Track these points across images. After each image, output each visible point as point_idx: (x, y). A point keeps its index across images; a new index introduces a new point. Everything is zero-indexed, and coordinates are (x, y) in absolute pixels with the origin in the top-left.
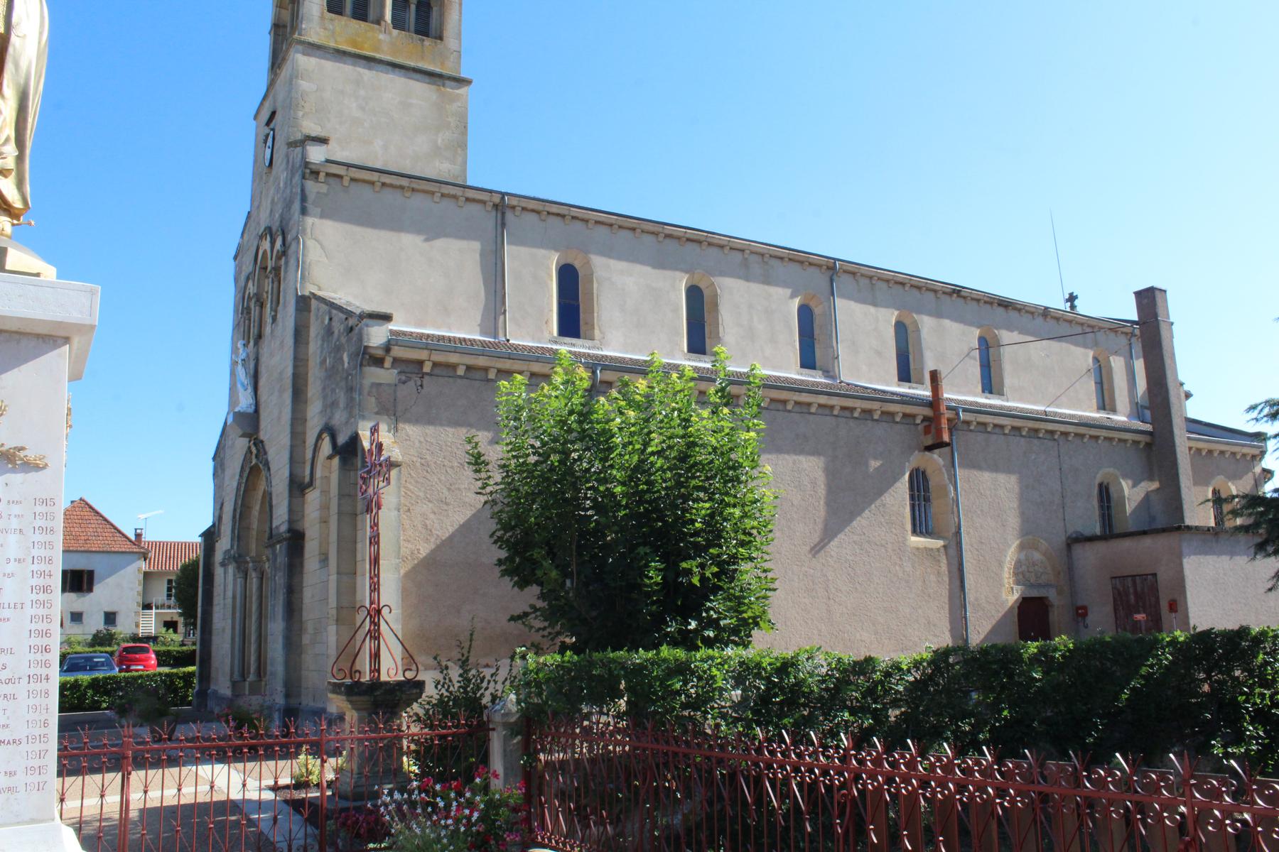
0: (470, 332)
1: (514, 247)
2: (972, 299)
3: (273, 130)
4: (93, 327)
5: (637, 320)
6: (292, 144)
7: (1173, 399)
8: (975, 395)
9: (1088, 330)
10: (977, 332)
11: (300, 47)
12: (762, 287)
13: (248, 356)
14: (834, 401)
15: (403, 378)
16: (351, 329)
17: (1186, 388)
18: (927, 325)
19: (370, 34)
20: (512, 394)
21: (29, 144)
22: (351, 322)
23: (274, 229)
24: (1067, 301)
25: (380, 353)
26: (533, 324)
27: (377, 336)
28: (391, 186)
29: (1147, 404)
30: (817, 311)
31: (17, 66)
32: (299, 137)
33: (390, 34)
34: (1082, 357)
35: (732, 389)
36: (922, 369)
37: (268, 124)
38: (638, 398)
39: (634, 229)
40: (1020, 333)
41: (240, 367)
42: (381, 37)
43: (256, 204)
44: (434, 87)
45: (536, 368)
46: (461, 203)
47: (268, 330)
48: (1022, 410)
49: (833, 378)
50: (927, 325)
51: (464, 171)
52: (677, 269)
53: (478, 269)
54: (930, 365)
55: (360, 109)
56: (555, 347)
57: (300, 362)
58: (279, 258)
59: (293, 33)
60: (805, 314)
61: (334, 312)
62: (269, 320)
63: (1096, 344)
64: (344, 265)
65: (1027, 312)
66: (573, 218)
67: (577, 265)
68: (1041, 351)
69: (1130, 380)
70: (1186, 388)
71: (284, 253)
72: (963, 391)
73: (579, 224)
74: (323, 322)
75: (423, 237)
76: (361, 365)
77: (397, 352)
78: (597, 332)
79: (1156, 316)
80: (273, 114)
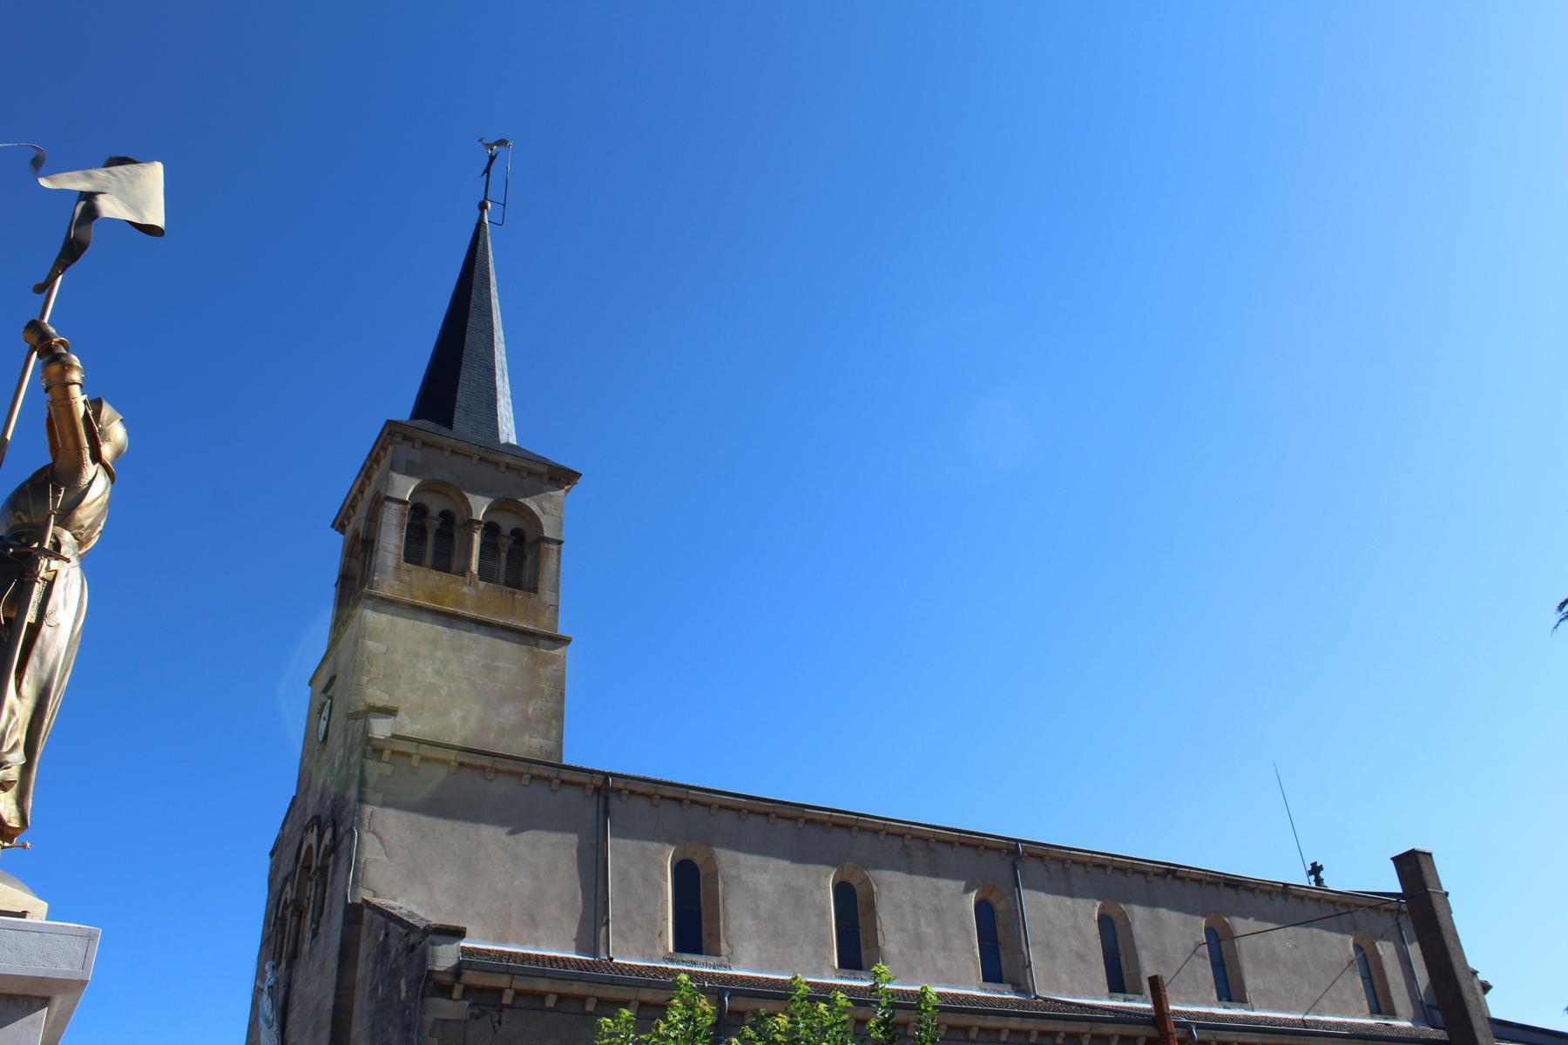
0: (560, 948)
1: (621, 841)
2: (1193, 880)
3: (331, 698)
4: (83, 983)
5: (775, 932)
6: (354, 716)
7: (1467, 995)
8: (1210, 1005)
9: (1342, 910)
10: (1203, 922)
11: (370, 602)
12: (928, 879)
13: (277, 981)
14: (1029, 1024)
15: (476, 1011)
16: (413, 948)
17: (1481, 977)
18: (1138, 915)
19: (452, 587)
20: (616, 1035)
21: (40, 749)
22: (413, 939)
23: (323, 819)
24: (1310, 873)
25: (448, 979)
26: (643, 942)
27: (445, 956)
28: (470, 766)
29: (1434, 1002)
30: (1000, 906)
31: (42, 659)
32: (361, 707)
33: (476, 585)
34: (1340, 945)
35: (901, 1016)
36: (1138, 975)
37: (325, 691)
38: (778, 1037)
39: (767, 814)
40: (1258, 919)
41: (265, 996)
42: (465, 589)
43: (304, 786)
44: (525, 647)
45: (647, 995)
46: (554, 787)
47: (306, 947)
48: (1273, 1021)
49: (1026, 992)
50: (1138, 915)
51: (560, 746)
52: (820, 862)
53: (574, 869)
54: (1148, 969)
55: (434, 679)
56: (670, 966)
57: (344, 990)
58: (326, 855)
59: (362, 585)
60: (984, 910)
61: (392, 925)
62: (308, 935)
63: (1352, 928)
64: (409, 870)
65: (1262, 891)
66: (692, 802)
67: (698, 860)
68: (1286, 941)
69: (1405, 968)
70: (1481, 977)
71: (334, 849)
72: (1194, 1002)
73: (699, 811)
74: (377, 938)
75: (507, 830)
76: (423, 995)
77: (470, 977)
78: (723, 946)
79: (1424, 886)
80: (332, 679)
